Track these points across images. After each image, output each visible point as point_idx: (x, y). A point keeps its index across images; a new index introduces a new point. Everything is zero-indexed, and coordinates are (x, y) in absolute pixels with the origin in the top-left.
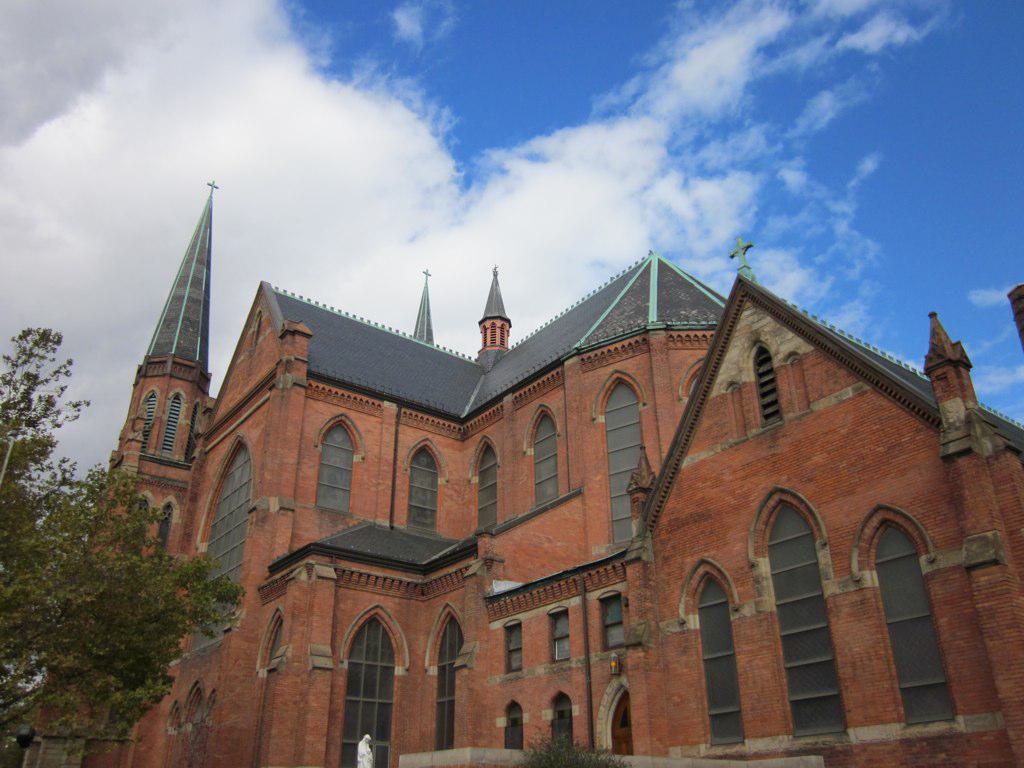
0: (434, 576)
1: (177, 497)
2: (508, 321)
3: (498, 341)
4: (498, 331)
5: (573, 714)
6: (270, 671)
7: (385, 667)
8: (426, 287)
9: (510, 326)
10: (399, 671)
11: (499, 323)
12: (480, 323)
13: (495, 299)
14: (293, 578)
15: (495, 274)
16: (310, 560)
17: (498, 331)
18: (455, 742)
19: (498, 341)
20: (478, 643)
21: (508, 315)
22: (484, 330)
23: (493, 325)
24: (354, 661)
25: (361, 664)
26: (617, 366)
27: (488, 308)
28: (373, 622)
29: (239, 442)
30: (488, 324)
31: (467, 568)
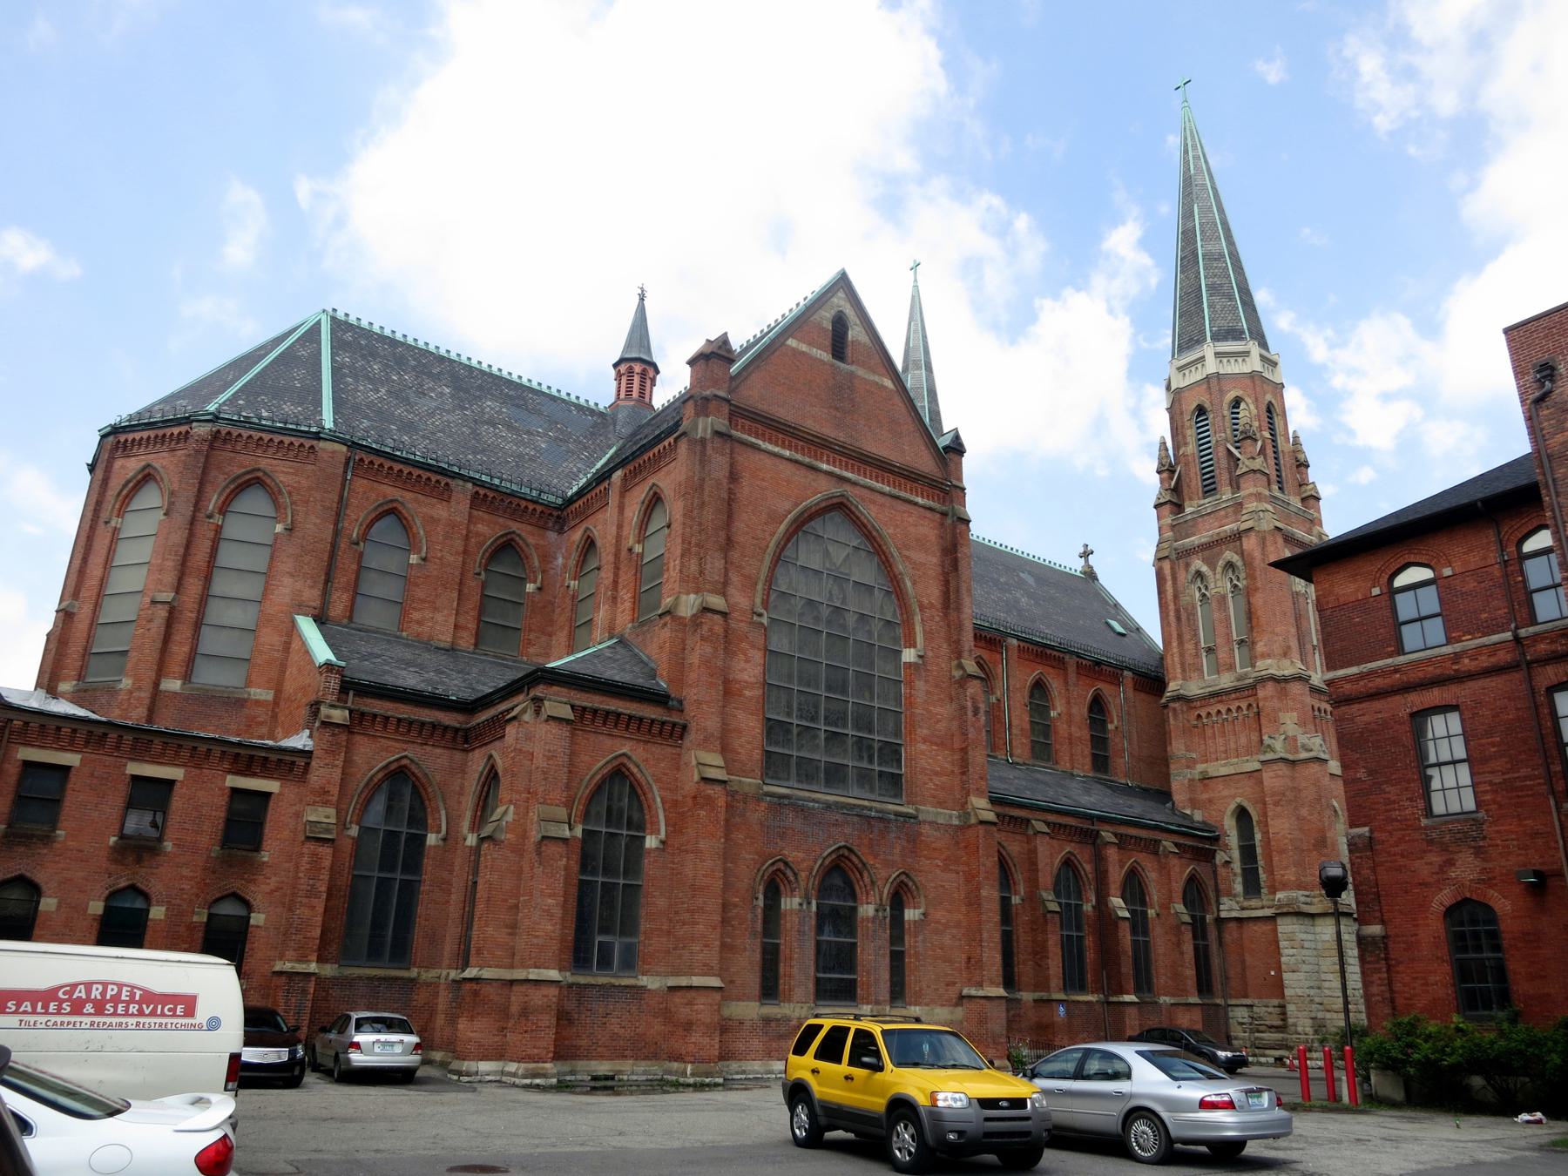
0: (483, 716)
1: (1206, 561)
2: (654, 366)
3: (635, 394)
4: (637, 379)
5: (40, 908)
6: (482, 840)
7: (611, 833)
8: (916, 287)
9: (657, 372)
10: (432, 839)
11: (638, 368)
12: (615, 366)
13: (640, 330)
14: (514, 718)
15: (642, 299)
16: (538, 691)
17: (637, 379)
18: (147, 937)
19: (635, 394)
20: (512, 807)
21: (656, 359)
22: (619, 376)
23: (630, 371)
24: (589, 828)
25: (402, 832)
26: (264, 463)
27: (629, 345)
28: (619, 774)
29: (655, 493)
30: (623, 368)
31: (509, 711)
